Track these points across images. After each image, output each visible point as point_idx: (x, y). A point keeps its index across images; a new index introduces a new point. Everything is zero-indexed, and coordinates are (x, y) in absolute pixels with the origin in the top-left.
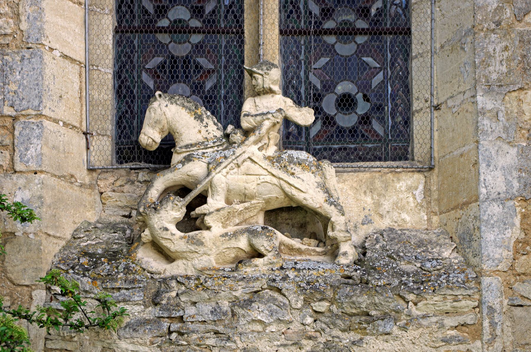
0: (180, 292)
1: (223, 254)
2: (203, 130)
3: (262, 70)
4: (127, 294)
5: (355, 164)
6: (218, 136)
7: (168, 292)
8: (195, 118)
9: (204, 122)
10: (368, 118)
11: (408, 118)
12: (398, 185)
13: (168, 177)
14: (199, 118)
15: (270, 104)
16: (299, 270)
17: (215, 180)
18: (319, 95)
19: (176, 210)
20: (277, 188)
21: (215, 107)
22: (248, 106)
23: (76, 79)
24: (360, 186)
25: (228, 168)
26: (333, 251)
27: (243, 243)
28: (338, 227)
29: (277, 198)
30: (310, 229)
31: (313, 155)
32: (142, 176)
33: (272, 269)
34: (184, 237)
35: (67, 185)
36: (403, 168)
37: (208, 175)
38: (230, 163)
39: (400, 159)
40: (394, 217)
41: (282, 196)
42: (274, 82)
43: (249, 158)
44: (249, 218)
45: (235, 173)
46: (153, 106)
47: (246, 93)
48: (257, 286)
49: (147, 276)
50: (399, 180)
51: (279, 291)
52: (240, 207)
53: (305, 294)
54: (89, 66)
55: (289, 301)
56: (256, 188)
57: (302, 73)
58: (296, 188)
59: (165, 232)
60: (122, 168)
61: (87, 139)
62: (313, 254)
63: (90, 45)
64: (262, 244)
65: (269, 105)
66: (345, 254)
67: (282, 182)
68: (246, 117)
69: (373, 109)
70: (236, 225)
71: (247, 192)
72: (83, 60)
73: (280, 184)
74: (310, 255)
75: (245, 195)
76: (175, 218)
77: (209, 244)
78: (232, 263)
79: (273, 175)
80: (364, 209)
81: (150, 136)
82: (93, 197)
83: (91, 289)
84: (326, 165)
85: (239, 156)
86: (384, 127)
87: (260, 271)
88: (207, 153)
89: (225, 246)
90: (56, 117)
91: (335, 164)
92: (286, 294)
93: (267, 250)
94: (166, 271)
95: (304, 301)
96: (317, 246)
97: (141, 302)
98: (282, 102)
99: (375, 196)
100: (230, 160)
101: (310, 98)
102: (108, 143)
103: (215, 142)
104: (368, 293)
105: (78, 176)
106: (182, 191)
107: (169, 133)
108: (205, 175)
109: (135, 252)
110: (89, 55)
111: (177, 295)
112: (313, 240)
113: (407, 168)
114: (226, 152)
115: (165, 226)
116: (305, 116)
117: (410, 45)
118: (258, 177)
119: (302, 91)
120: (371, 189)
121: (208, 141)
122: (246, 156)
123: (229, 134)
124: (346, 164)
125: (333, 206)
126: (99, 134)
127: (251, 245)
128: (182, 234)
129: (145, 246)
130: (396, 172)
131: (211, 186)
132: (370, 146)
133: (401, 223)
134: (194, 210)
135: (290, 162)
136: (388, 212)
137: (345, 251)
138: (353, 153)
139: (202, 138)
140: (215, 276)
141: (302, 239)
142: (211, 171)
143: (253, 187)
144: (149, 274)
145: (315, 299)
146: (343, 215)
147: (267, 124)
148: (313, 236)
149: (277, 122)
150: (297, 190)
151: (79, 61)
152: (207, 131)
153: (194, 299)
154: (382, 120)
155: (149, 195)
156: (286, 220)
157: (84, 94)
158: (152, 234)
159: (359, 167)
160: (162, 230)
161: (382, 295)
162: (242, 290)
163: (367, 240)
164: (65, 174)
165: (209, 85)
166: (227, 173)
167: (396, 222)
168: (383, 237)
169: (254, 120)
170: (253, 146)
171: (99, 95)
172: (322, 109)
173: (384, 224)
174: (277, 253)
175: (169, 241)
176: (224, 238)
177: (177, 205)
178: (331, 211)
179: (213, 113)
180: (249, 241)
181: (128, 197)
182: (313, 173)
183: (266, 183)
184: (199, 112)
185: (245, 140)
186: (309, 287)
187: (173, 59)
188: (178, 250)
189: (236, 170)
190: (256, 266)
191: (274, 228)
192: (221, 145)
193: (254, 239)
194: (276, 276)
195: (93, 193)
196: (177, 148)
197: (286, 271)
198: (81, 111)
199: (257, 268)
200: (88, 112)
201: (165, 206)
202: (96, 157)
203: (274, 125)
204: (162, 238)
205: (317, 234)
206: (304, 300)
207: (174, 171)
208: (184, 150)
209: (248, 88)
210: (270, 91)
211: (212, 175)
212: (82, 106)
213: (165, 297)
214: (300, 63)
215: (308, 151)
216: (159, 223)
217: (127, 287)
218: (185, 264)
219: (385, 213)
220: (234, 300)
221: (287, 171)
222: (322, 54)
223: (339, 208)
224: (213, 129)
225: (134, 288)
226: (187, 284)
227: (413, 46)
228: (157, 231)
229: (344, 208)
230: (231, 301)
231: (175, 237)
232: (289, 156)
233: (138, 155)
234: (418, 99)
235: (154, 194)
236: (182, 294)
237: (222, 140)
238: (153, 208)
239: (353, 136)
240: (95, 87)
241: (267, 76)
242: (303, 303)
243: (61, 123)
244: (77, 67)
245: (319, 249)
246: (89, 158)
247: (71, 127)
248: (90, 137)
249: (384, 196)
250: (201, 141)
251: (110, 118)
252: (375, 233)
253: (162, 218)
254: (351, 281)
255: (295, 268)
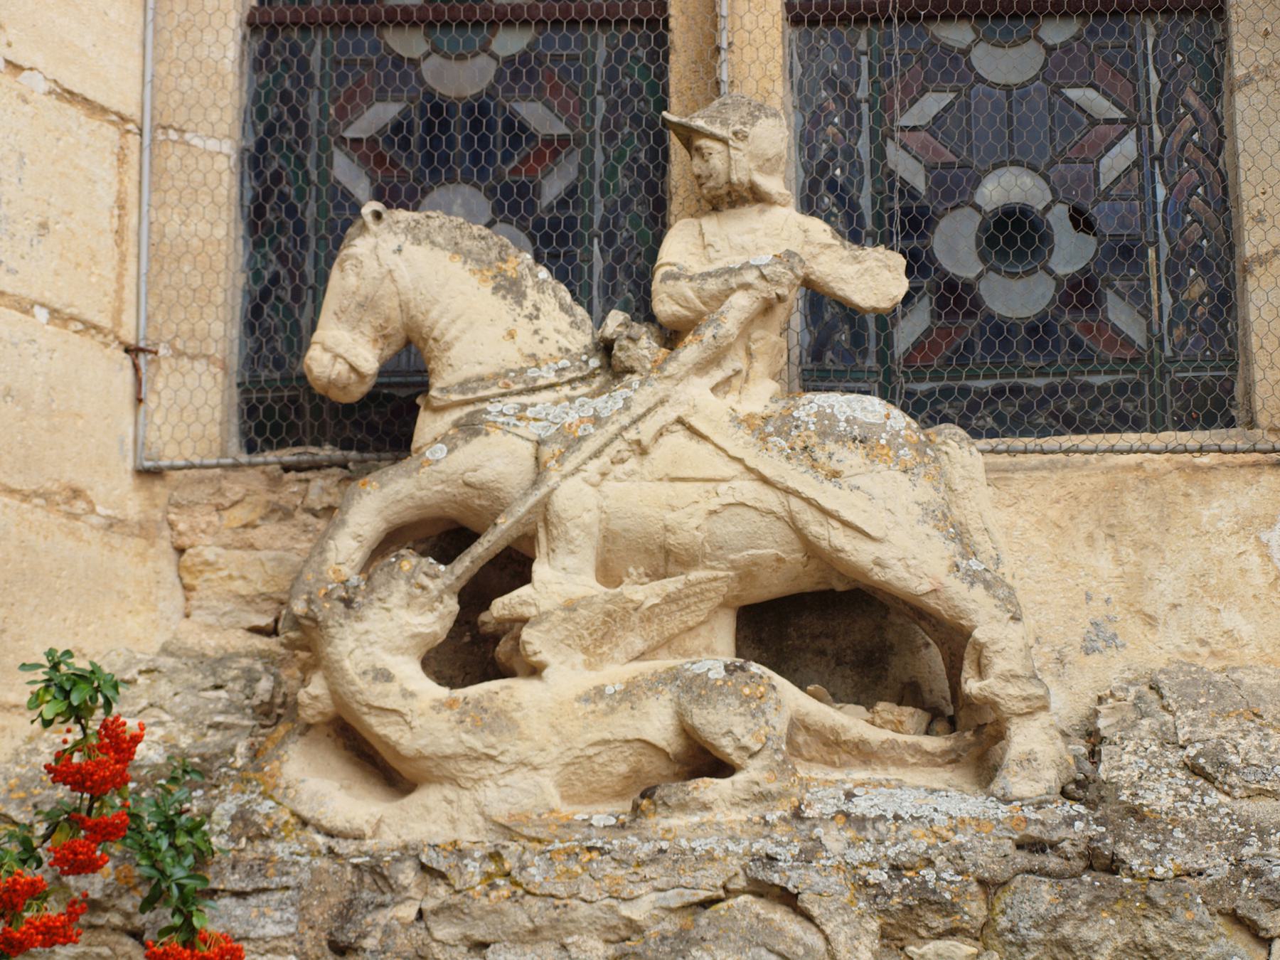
0: (429, 904)
1: (586, 763)
2: (524, 329)
3: (725, 123)
4: (239, 912)
5: (1051, 442)
6: (574, 350)
7: (383, 906)
8: (496, 289)
9: (528, 304)
10: (1091, 283)
11: (1231, 282)
12: (1206, 513)
13: (397, 493)
14: (509, 291)
15: (752, 244)
16: (860, 822)
17: (561, 502)
18: (923, 210)
19: (423, 606)
20: (779, 524)
21: (570, 257)
22: (678, 247)
23: (105, 170)
24: (1072, 518)
25: (605, 459)
26: (975, 737)
27: (657, 723)
28: (1000, 665)
29: (779, 560)
30: (897, 669)
31: (904, 408)
32: (319, 488)
33: (763, 818)
34: (451, 704)
35: (56, 519)
36: (1220, 451)
37: (535, 483)
38: (611, 441)
39: (1209, 423)
40: (1196, 625)
41: (796, 557)
42: (768, 165)
43: (680, 421)
44: (681, 632)
45: (631, 474)
46: (351, 251)
47: (674, 207)
48: (708, 881)
49: (315, 843)
50: (1207, 493)
51: (788, 899)
52: (644, 593)
53: (886, 912)
54: (154, 129)
55: (827, 939)
56: (705, 527)
57: (864, 146)
58: (846, 524)
59: (379, 687)
60: (252, 465)
61: (136, 368)
62: (912, 760)
63: (158, 61)
64: (724, 724)
65: (747, 239)
66: (1028, 760)
67: (796, 504)
68: (670, 282)
69: (1108, 252)
70: (636, 659)
71: (672, 540)
72: (131, 110)
73: (790, 512)
74: (901, 763)
75: (667, 552)
76: (414, 636)
77: (535, 726)
78: (619, 795)
79: (765, 480)
80: (1089, 598)
81: (342, 351)
82: (150, 564)
83: (109, 896)
84: (951, 437)
85: (644, 415)
86: (1146, 317)
87: (718, 824)
88: (534, 405)
89: (595, 736)
90: (22, 291)
91: (983, 443)
92: (815, 911)
93: (744, 748)
94: (384, 827)
95: (882, 937)
96: (927, 733)
97: (288, 944)
98: (795, 230)
99: (1127, 552)
100: (612, 429)
101: (891, 218)
102: (207, 382)
103: (563, 369)
104: (1117, 907)
105: (98, 492)
106: (443, 535)
107: (408, 343)
108: (527, 483)
109: (278, 758)
110: (153, 97)
111: (421, 915)
112: (910, 709)
113: (1235, 451)
114: (599, 402)
115: (379, 665)
116: (873, 279)
117: (1223, 44)
118: (710, 486)
119: (865, 201)
120: (1111, 526)
121: (537, 366)
122: (666, 415)
123: (613, 341)
124: (1020, 443)
125: (979, 590)
126: (179, 354)
127: (688, 733)
128: (443, 692)
129: (311, 733)
130: (1197, 468)
131: (546, 522)
132: (1098, 380)
133: (1220, 647)
134: (486, 606)
135: (823, 434)
136: (1175, 606)
137: (1027, 748)
138: (1043, 403)
139: (517, 357)
140: (558, 845)
141: (869, 707)
142: (547, 469)
143: (694, 522)
144: (320, 839)
145: (923, 932)
146: (1016, 618)
147: (741, 304)
148: (910, 694)
149: (778, 296)
150: (849, 532)
151: (117, 113)
152: (536, 332)
153: (478, 934)
154: (1139, 298)
155: (331, 555)
156: (815, 637)
157: (132, 220)
158: (334, 693)
159: (1067, 452)
160: (369, 677)
161: (1171, 916)
162: (654, 896)
163: (1102, 709)
164: (48, 485)
165: (552, 188)
166: (604, 475)
167: (1203, 643)
168: (1162, 697)
169: (699, 293)
170: (695, 380)
171: (183, 223)
172: (931, 258)
173: (1155, 651)
174: (779, 757)
175: (394, 718)
176: (591, 707)
177: (423, 588)
178: (972, 606)
179: (561, 276)
180: (681, 716)
181: (269, 565)
182: (905, 472)
183: (739, 510)
184: (510, 268)
185: (665, 361)
186: (899, 885)
187: (436, 110)
188: (428, 751)
189: (632, 464)
190: (706, 807)
191: (771, 668)
192: (583, 379)
193: (696, 711)
194: (779, 844)
195: (152, 551)
196: (433, 393)
197: (815, 826)
198: (120, 276)
199: (707, 816)
200: (143, 278)
201: (382, 593)
202: (166, 429)
203: (768, 308)
204: (370, 707)
205: (926, 688)
206: (884, 935)
207: (417, 470)
208: (455, 397)
209: (681, 191)
210: (756, 196)
211: (551, 483)
212: (123, 259)
213: (375, 925)
214: (856, 105)
215: (887, 394)
216: (358, 653)
217: (238, 886)
218: (450, 802)
219: (1161, 610)
220: (624, 933)
221: (814, 464)
222: (929, 78)
223: (1002, 592)
224: (555, 325)
225: (265, 890)
226: (453, 875)
227: (1237, 44)
228: (352, 683)
229: (1019, 594)
230: (613, 937)
231: (415, 704)
232: (820, 415)
233: (321, 424)
234: (1259, 219)
235: (347, 548)
236: (435, 913)
237: (586, 362)
238: (342, 600)
239: (1041, 345)
240: (172, 197)
241: (741, 145)
242: (877, 946)
243: (42, 314)
244: (111, 132)
245: (933, 743)
246: (141, 433)
247: (80, 326)
248: (148, 363)
249: (1158, 550)
250: (516, 367)
251: (219, 297)
252: (1130, 683)
253: (372, 637)
254: (1053, 862)
255: (847, 815)
